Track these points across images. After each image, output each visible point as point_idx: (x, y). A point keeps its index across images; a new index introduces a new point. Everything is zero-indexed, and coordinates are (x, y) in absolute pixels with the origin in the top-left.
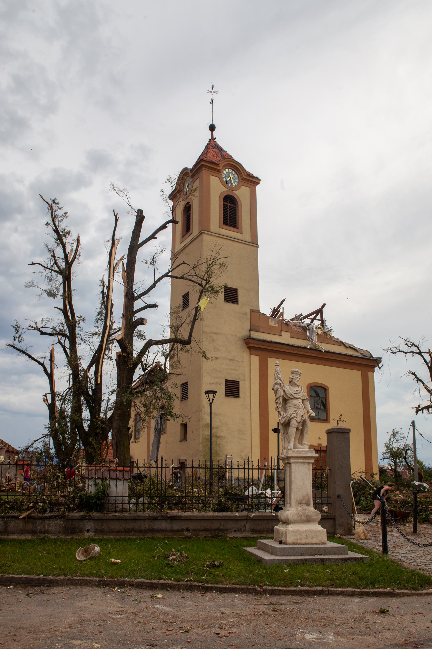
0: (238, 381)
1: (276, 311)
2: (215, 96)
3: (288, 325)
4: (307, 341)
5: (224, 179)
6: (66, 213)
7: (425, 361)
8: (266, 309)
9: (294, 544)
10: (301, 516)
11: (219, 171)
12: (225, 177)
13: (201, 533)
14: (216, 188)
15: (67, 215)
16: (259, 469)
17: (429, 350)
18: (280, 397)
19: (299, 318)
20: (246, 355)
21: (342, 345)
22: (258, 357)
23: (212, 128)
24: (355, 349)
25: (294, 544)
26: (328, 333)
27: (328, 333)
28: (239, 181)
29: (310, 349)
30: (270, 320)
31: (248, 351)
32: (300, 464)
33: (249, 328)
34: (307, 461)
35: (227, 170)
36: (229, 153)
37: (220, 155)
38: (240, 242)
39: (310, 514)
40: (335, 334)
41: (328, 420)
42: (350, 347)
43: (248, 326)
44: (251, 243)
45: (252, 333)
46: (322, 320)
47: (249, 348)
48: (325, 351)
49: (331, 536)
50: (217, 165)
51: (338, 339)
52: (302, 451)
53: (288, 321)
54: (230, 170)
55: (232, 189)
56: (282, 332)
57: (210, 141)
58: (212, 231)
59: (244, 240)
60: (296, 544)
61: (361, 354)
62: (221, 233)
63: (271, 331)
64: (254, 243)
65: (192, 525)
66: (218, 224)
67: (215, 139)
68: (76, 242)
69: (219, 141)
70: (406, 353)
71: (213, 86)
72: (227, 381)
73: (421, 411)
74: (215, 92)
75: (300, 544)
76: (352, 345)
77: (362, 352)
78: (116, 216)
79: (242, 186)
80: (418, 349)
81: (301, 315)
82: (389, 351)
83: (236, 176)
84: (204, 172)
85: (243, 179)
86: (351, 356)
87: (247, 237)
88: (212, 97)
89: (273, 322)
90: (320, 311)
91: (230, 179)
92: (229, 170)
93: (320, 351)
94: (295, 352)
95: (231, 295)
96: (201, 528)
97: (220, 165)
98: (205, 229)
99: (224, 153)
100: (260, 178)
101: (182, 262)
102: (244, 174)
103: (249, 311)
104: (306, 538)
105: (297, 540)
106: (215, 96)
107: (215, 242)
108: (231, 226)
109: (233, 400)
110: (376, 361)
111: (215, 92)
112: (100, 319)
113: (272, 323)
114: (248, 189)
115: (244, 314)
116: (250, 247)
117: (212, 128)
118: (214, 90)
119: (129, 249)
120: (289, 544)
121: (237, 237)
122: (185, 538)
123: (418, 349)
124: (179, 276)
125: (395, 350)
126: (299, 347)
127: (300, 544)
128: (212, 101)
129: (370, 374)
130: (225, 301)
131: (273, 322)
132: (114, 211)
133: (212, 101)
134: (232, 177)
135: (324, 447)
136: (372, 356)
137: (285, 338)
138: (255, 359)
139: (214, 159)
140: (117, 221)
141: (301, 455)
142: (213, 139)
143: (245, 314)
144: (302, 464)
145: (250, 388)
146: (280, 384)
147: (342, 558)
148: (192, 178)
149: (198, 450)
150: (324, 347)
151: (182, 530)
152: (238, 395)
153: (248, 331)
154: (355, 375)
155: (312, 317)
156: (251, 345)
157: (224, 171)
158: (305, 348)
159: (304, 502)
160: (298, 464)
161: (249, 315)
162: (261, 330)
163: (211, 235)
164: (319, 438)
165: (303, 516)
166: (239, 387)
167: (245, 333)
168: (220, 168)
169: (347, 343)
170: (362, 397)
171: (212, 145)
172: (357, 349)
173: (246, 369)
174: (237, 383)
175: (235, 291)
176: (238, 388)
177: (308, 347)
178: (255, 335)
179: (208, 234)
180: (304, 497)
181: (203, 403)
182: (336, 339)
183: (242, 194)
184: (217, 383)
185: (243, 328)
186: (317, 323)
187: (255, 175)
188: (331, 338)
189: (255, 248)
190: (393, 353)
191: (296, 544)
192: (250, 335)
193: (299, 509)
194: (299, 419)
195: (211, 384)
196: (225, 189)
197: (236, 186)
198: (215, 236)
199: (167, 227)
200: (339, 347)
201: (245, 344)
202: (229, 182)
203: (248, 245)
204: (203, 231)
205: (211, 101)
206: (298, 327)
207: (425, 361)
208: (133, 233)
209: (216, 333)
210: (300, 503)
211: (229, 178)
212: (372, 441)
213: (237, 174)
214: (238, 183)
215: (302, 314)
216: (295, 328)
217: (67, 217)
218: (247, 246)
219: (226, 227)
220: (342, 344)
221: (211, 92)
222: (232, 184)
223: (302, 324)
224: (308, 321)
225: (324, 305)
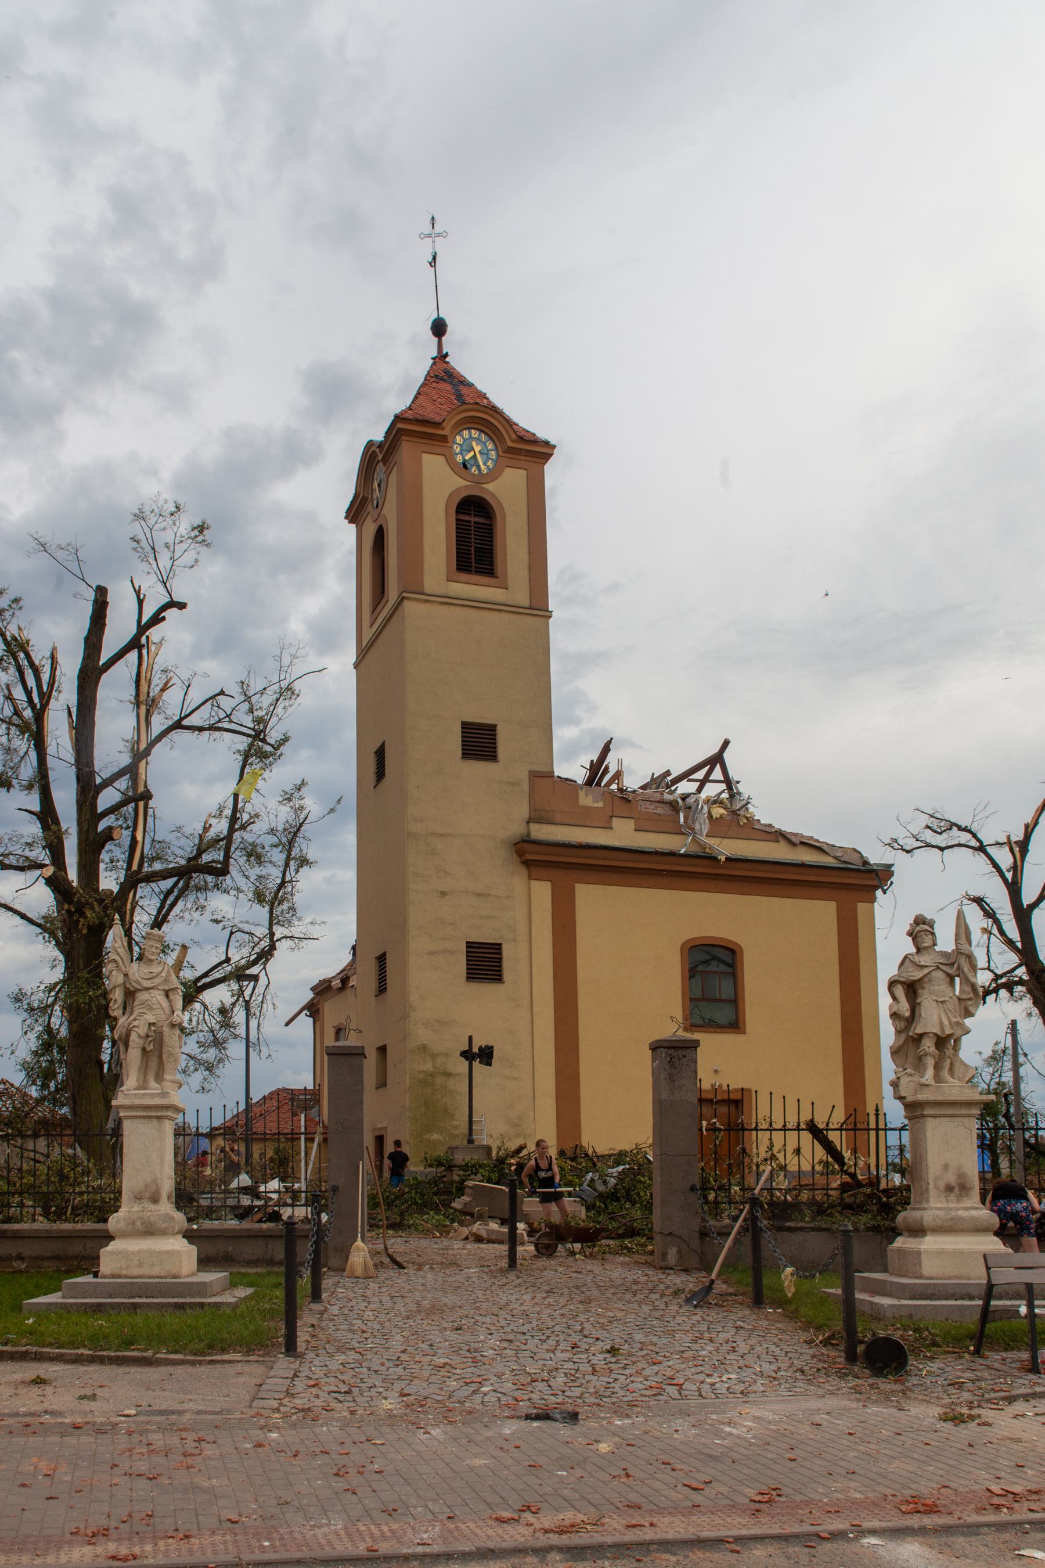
0: (500, 945)
1: (596, 770)
2: (441, 246)
3: (630, 801)
4: (683, 837)
5: (459, 459)
6: (16, 601)
7: (995, 865)
8: (572, 768)
9: (113, 1276)
10: (134, 1223)
11: (444, 439)
12: (461, 453)
13: (46, 1263)
14: (438, 482)
15: (21, 603)
17: (1008, 838)
18: (115, 987)
19: (661, 782)
20: (517, 881)
21: (781, 839)
22: (549, 884)
23: (439, 328)
24: (818, 848)
25: (113, 1276)
26: (742, 812)
27: (742, 812)
28: (498, 456)
30: (582, 794)
31: (524, 871)
32: (140, 1121)
33: (527, 816)
34: (154, 1114)
35: (466, 433)
36: (479, 388)
37: (453, 397)
38: (500, 610)
39: (152, 1219)
40: (763, 813)
41: (741, 1025)
42: (802, 843)
43: (523, 811)
44: (530, 608)
45: (533, 827)
46: (728, 781)
47: (526, 863)
48: (728, 859)
49: (205, 1262)
50: (438, 425)
52: (144, 1094)
53: (634, 791)
54: (473, 432)
55: (480, 479)
56: (614, 819)
57: (434, 364)
58: (427, 591)
59: (510, 603)
60: (119, 1276)
61: (835, 858)
62: (452, 594)
63: (585, 818)
64: (538, 607)
65: (28, 1249)
66: (444, 570)
67: (447, 355)
68: (49, 662)
69: (459, 363)
70: (942, 849)
71: (433, 218)
72: (470, 945)
73: (994, 995)
74: (439, 235)
75: (126, 1277)
76: (812, 838)
77: (839, 854)
78: (138, 593)
79: (508, 470)
80: (974, 836)
81: (668, 773)
82: (895, 845)
83: (490, 446)
84: (406, 448)
85: (510, 451)
86: (803, 865)
87: (520, 594)
88: (434, 247)
89: (590, 797)
90: (717, 759)
91: (475, 456)
92: (470, 434)
93: (715, 859)
95: (479, 742)
96: (47, 1254)
97: (444, 424)
98: (413, 589)
99: (464, 390)
100: (553, 442)
101: (218, 691)
102: (510, 437)
103: (524, 776)
104: (140, 1265)
105: (121, 1268)
106: (441, 246)
107: (446, 618)
108: (479, 572)
109: (486, 990)
110: (877, 875)
111: (439, 235)
112: (125, 825)
113: (586, 799)
114: (523, 473)
115: (512, 784)
116: (528, 618)
117: (439, 328)
118: (438, 229)
119: (79, 677)
120: (105, 1277)
122: (15, 1272)
123: (974, 836)
124: (206, 724)
125: (911, 843)
126: (657, 853)
127: (126, 1277)
128: (434, 258)
129: (861, 907)
130: (463, 758)
131: (590, 797)
132: (132, 581)
133: (434, 258)
134: (477, 448)
135: (707, 1091)
136: (866, 863)
137: (623, 834)
138: (542, 891)
139: (447, 409)
141: (137, 1102)
142: (442, 357)
143: (515, 784)
144: (146, 1121)
145: (530, 961)
146: (115, 961)
147: (176, 1303)
148: (384, 464)
149: (403, 1107)
150: (725, 848)
151: (9, 1258)
152: (500, 975)
153: (525, 824)
154: (822, 913)
155: (700, 775)
156: (529, 857)
157: (458, 438)
158: (672, 854)
159: (147, 1194)
160: (135, 1120)
161: (525, 786)
162: (558, 818)
163: (426, 601)
164: (716, 1071)
165: (138, 1223)
166: (501, 959)
167: (516, 828)
169: (795, 835)
170: (837, 966)
171: (443, 375)
172: (825, 847)
173: (521, 913)
174: (497, 947)
175: (490, 730)
176: (500, 960)
177: (682, 851)
178: (542, 832)
179: (418, 600)
180: (146, 1186)
181: (411, 998)
182: (765, 825)
183: (506, 489)
184: (445, 951)
185: (511, 818)
186: (711, 790)
187: (542, 434)
188: (751, 820)
189: (542, 620)
190: (908, 852)
191: (119, 1276)
192: (529, 833)
193: (136, 1209)
194: (143, 1030)
195: (431, 953)
198: (435, 602)
199: (164, 619)
200: (773, 845)
201: (515, 856)
202: (472, 462)
203: (521, 613)
204: (404, 594)
205: (430, 259)
206: (661, 801)
207: (995, 865)
208: (87, 639)
209: (441, 835)
210: (138, 1198)
211: (472, 453)
212: (867, 1075)
214: (496, 462)
215: (668, 771)
216: (651, 808)
217: (20, 608)
218: (520, 616)
219: (464, 576)
221: (429, 236)
222: (478, 467)
223: (667, 797)
224: (686, 787)
225: (726, 743)
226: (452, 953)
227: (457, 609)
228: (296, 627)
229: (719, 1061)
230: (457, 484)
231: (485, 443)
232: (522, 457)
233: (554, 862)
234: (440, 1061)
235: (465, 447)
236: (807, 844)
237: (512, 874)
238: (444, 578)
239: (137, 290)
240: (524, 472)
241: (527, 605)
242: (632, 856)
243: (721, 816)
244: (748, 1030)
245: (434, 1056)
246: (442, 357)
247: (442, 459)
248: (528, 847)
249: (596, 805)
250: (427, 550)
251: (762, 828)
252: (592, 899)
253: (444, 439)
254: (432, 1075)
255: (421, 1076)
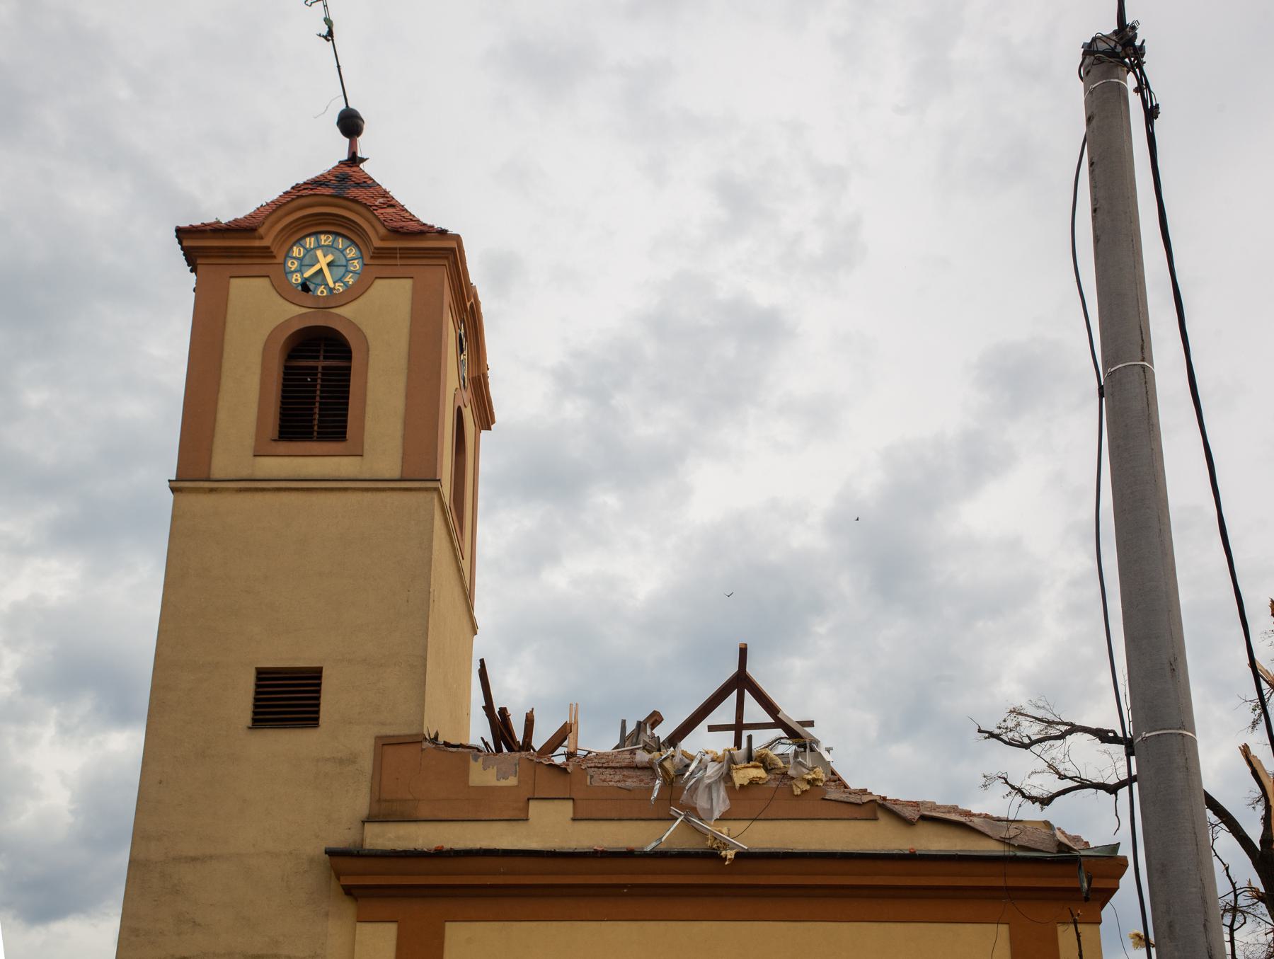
5: (296, 279)
21: (880, 814)
24: (961, 824)
31: (349, 908)
38: (346, 489)
42: (924, 818)
45: (371, 829)
47: (349, 891)
48: (741, 856)
51: (864, 791)
54: (323, 237)
59: (367, 476)
61: (1003, 841)
63: (481, 807)
76: (954, 809)
79: (233, 281)
81: (655, 719)
85: (380, 254)
86: (912, 857)
90: (741, 682)
91: (321, 270)
92: (318, 241)
94: (615, 880)
102: (377, 232)
103: (365, 748)
107: (320, 511)
115: (341, 762)
117: (350, 124)
121: (336, 474)
137: (551, 827)
142: (354, 160)
163: (212, 490)
168: (266, 242)
172: (977, 823)
182: (855, 793)
198: (227, 490)
209: (194, 859)
213: (357, 246)
220: (877, 808)
225: (743, 652)
227: (268, 497)
231: (342, 251)
232: (399, 262)
235: (306, 261)
237: (327, 915)
238: (251, 453)
239: (763, 295)
240: (409, 282)
241: (397, 475)
243: (753, 783)
247: (265, 282)
249: (503, 783)
251: (853, 799)
253: (266, 253)
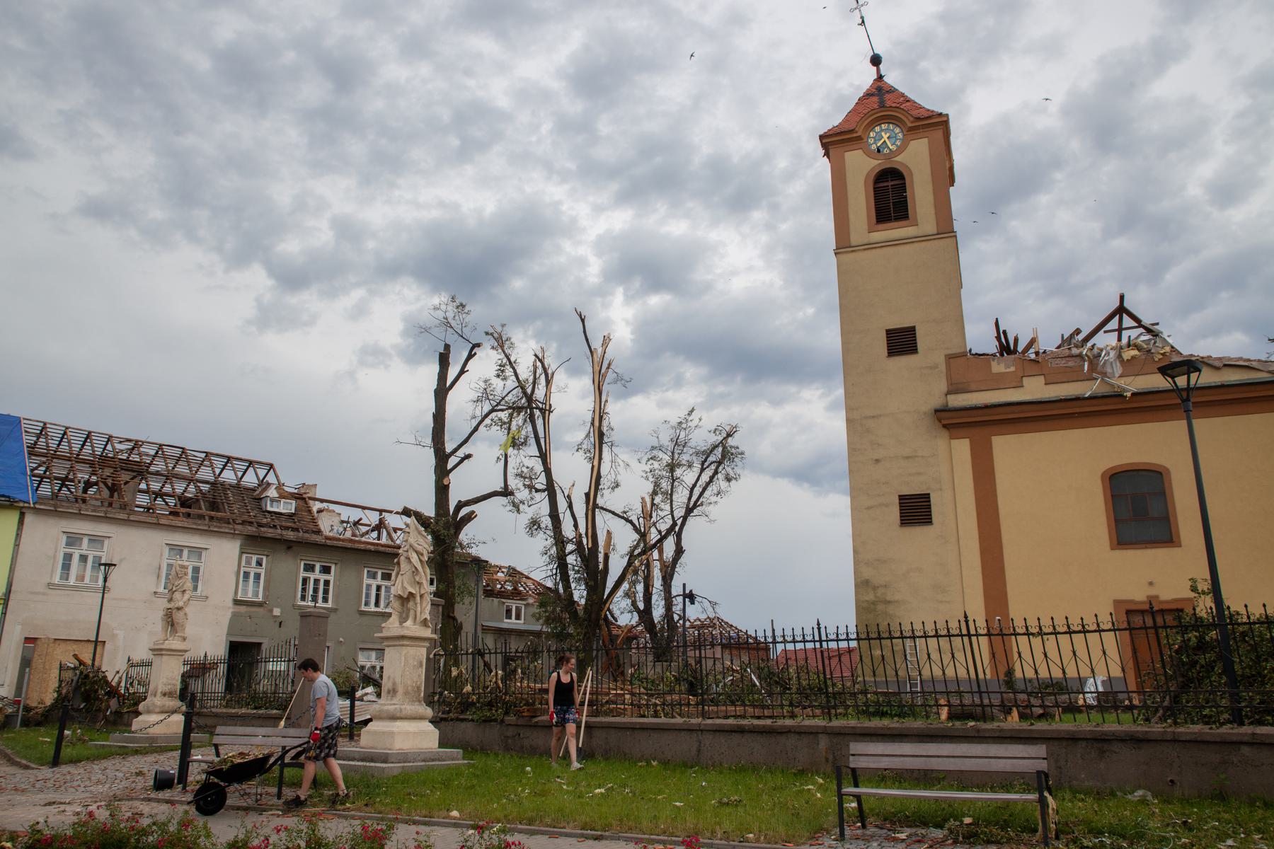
5: (874, 147)
16: (1114, 630)
20: (941, 442)
29: (1090, 398)
31: (945, 433)
45: (950, 397)
47: (945, 426)
50: (852, 131)
58: (853, 242)
61: (1269, 372)
63: (999, 382)
69: (891, 79)
72: (901, 498)
76: (1241, 359)
81: (1078, 331)
83: (897, 130)
85: (911, 129)
90: (1121, 310)
100: (945, 112)
107: (898, 251)
108: (897, 219)
109: (918, 532)
113: (998, 367)
115: (931, 368)
117: (876, 61)
137: (1035, 389)
138: (962, 448)
140: (583, 321)
156: (945, 422)
158: (1077, 399)
161: (943, 367)
164: (1151, 584)
167: (937, 402)
169: (1220, 359)
172: (1254, 364)
173: (947, 469)
178: (958, 401)
183: (915, 157)
185: (934, 393)
195: (869, 508)
196: (877, 162)
197: (899, 148)
216: (1062, 363)
225: (1122, 297)
226: (887, 506)
228: (1194, 191)
229: (85, 541)
230: (873, 164)
233: (964, 421)
234: (880, 592)
236: (1230, 365)
242: (1039, 407)
243: (1133, 357)
244: (1183, 543)
245: (875, 588)
246: (880, 77)
248: (943, 414)
250: (851, 216)
252: (1009, 449)
253: (859, 138)
254: (874, 603)
255: (865, 605)
